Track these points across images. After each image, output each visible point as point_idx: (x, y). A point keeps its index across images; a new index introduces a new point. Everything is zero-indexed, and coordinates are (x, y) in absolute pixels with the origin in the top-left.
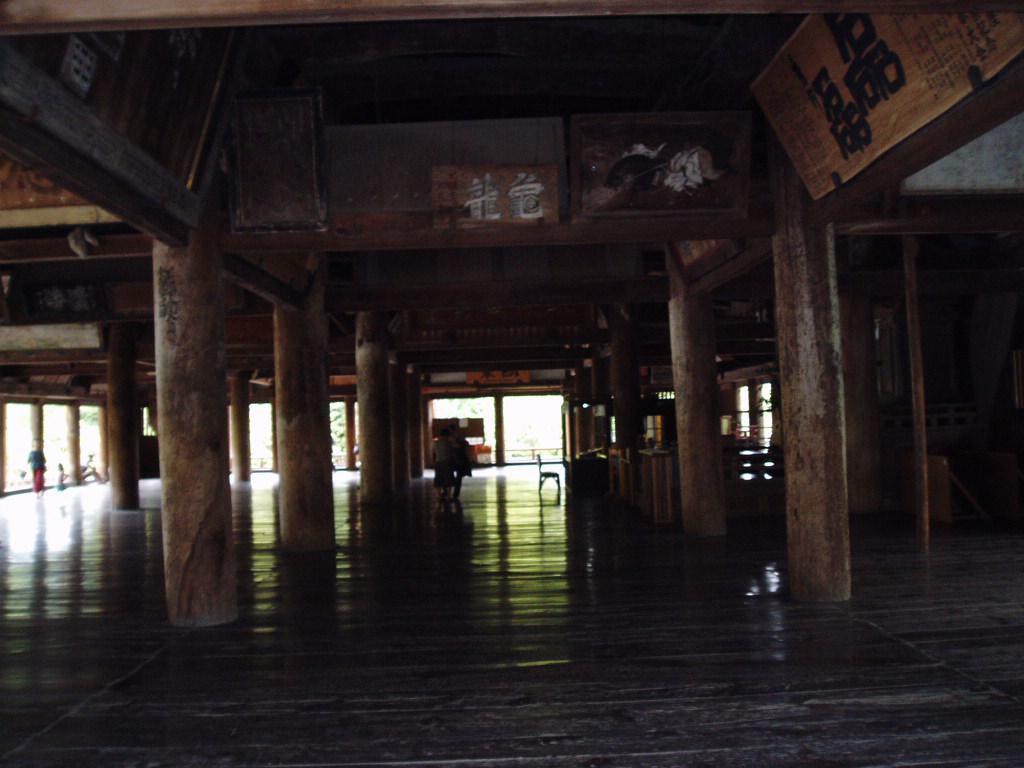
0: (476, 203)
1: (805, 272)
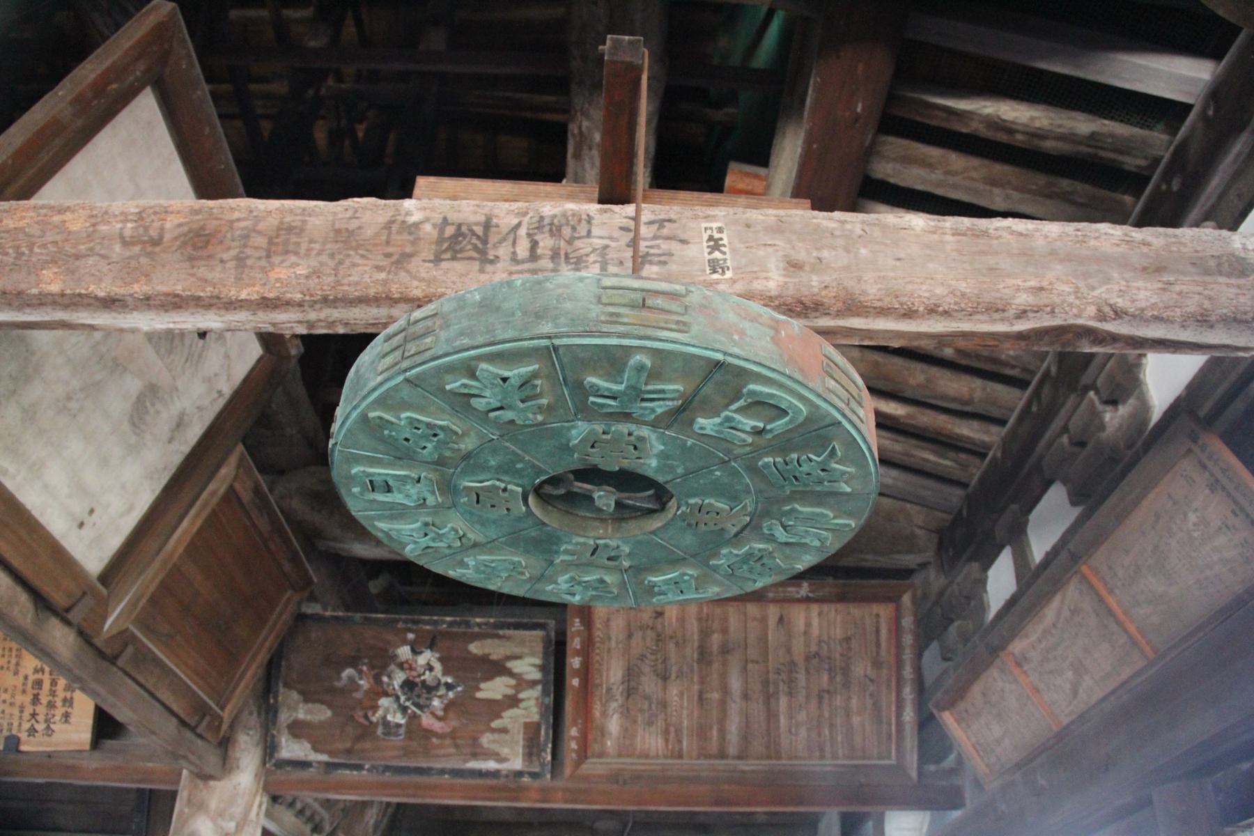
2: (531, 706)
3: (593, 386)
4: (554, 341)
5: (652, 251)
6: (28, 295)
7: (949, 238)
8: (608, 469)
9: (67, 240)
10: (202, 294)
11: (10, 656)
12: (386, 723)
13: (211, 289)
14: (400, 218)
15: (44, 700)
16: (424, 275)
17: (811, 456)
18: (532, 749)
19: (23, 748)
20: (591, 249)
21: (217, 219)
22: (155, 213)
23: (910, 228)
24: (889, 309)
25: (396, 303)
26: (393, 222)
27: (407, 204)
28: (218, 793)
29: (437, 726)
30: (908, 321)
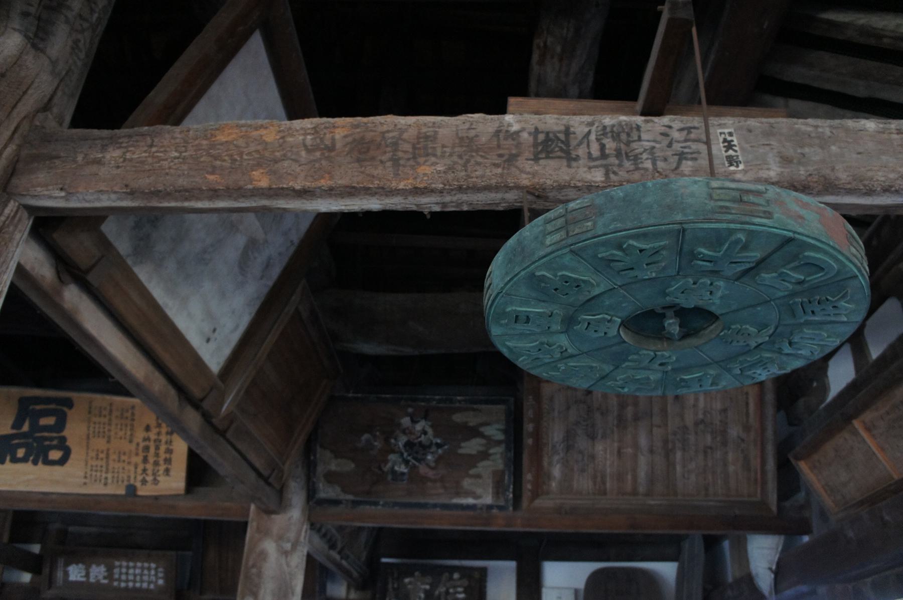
2: (497, 459)
3: (700, 253)
4: (684, 225)
5: (686, 150)
6: (246, 189)
7: (895, 136)
8: (687, 307)
9: (266, 149)
10: (371, 186)
11: (126, 430)
12: (393, 472)
13: (378, 182)
14: (504, 129)
15: (151, 460)
16: (528, 170)
17: (828, 297)
18: (498, 489)
19: (140, 493)
20: (642, 150)
21: (372, 131)
22: (326, 128)
23: (865, 130)
24: (856, 189)
25: (510, 189)
26: (500, 131)
27: (508, 118)
28: (279, 521)
29: (431, 474)
30: (867, 197)
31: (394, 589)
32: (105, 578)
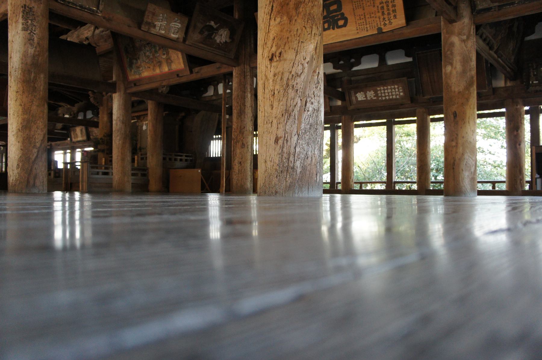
0: (158, 24)
1: (249, 81)
15: (386, 13)
19: (384, 31)
28: (457, 26)
31: (534, 75)
32: (374, 96)
